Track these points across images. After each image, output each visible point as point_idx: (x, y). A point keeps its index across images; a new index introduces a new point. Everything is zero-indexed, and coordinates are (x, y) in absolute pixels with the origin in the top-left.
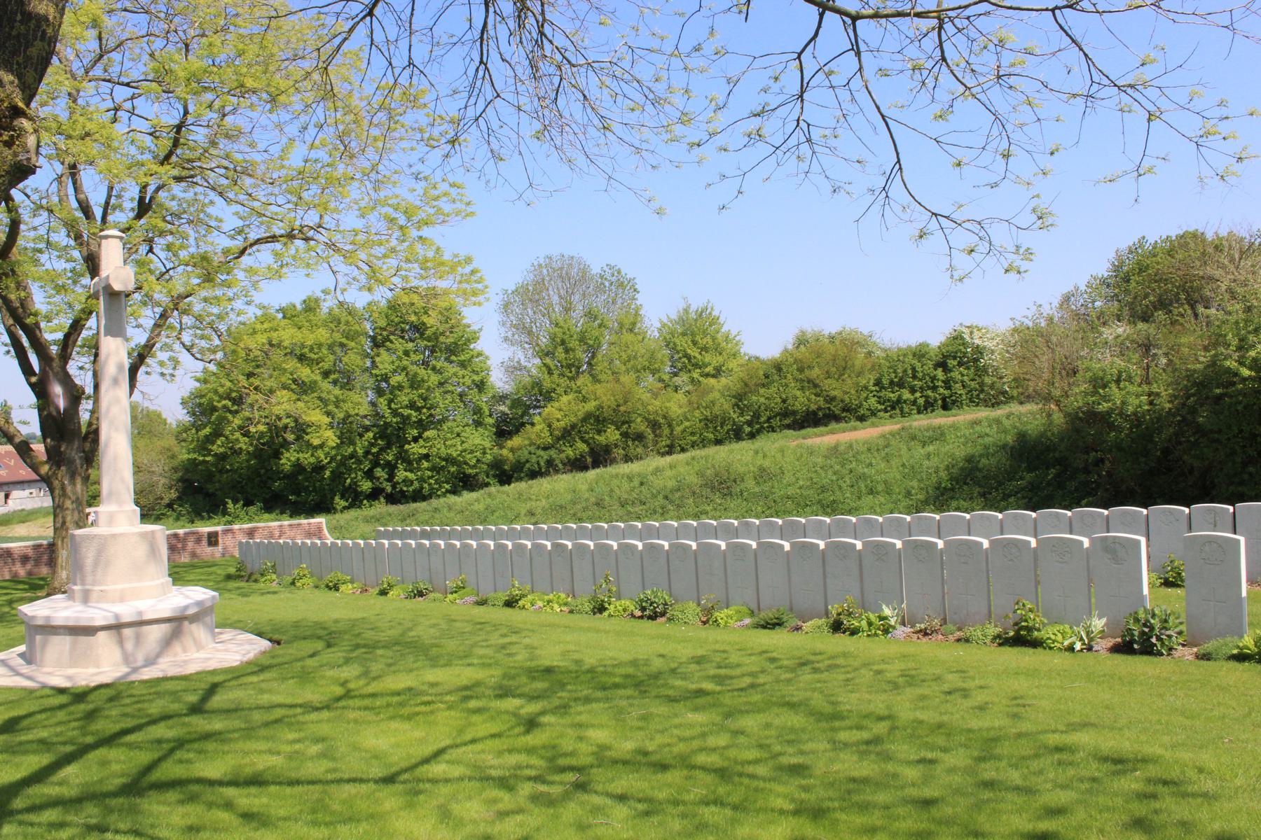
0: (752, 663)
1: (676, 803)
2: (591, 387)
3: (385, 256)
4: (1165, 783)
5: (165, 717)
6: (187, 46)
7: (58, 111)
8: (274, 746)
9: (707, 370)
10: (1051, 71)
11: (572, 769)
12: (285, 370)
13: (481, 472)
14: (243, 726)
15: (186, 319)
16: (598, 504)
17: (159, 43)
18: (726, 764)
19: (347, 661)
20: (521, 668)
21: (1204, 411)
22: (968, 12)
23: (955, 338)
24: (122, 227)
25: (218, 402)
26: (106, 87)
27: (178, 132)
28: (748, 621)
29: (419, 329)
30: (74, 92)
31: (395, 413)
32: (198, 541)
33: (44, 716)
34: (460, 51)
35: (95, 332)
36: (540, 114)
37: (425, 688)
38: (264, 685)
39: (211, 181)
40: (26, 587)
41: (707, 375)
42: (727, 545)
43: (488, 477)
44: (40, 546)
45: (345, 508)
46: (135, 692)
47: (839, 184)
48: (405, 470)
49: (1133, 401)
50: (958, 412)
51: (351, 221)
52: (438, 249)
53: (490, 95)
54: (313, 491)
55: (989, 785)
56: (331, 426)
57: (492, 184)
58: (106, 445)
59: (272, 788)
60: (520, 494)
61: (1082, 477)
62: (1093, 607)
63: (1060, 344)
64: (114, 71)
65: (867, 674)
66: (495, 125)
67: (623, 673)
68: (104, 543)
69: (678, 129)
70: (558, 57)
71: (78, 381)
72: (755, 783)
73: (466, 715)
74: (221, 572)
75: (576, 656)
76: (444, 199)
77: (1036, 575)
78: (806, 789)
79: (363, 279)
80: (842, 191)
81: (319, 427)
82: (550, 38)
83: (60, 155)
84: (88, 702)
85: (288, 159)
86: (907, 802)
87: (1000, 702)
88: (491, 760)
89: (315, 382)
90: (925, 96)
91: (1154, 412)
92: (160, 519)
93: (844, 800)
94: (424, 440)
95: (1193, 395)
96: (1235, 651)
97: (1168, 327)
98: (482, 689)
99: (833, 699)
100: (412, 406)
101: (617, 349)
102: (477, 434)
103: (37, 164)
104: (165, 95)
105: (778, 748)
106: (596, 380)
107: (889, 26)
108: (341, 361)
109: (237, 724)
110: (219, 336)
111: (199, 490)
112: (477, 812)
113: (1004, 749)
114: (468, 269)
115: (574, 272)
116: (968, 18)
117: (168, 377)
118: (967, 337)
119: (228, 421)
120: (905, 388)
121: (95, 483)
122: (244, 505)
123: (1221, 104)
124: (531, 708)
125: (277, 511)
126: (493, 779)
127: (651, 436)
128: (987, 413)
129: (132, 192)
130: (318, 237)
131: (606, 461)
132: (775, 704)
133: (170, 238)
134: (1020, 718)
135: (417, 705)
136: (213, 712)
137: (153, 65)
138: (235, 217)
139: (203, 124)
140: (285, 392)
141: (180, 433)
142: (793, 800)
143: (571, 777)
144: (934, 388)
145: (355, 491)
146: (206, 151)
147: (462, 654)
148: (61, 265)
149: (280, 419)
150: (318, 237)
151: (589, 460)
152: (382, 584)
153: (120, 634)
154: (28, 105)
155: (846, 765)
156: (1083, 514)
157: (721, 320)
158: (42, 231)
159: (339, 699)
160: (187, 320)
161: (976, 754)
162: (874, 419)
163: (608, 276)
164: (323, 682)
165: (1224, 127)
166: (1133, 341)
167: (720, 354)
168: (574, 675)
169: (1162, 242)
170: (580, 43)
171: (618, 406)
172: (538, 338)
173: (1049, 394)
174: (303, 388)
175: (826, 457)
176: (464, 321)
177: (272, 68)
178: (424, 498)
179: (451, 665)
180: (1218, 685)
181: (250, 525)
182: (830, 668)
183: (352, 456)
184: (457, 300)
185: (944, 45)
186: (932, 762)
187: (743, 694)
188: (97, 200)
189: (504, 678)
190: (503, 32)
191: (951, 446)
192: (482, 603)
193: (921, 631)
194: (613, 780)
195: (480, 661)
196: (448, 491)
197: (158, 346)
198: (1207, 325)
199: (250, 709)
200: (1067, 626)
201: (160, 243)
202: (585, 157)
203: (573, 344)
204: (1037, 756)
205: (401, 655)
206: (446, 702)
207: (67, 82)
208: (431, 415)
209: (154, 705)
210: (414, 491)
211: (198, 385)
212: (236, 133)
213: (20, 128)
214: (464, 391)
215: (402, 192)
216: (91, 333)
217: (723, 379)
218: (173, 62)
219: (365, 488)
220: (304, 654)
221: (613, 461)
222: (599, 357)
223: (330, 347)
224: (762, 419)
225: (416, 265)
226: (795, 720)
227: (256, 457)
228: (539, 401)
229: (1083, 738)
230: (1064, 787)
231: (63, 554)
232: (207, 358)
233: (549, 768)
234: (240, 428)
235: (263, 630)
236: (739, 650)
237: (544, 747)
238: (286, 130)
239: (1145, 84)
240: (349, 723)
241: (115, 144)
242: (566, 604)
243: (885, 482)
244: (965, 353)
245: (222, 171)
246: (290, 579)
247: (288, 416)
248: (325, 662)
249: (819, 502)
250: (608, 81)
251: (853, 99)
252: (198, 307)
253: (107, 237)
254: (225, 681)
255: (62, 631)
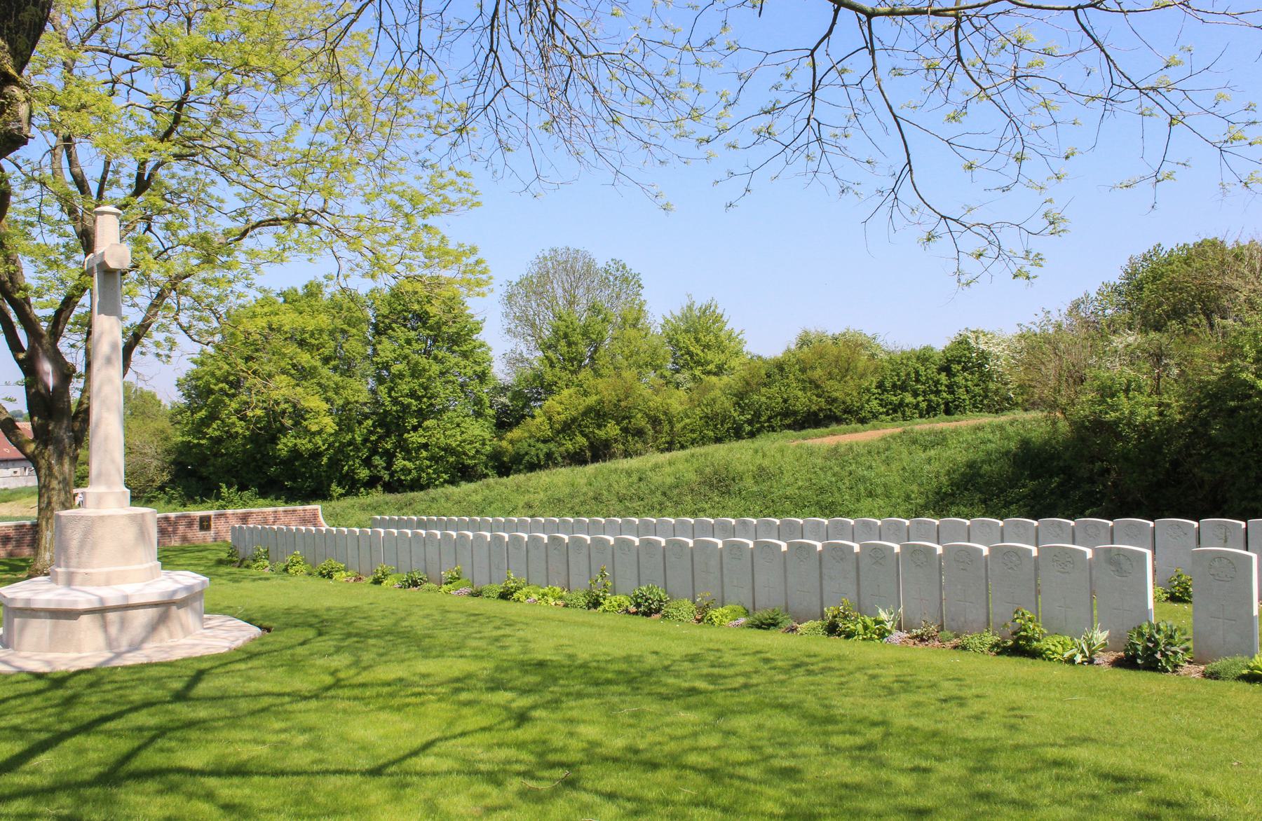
0: (746, 664)
1: (665, 803)
2: (592, 382)
3: (389, 243)
4: (1169, 804)
5: (147, 704)
6: (189, 20)
7: (52, 80)
8: (259, 735)
9: (709, 368)
10: (1071, 74)
11: (562, 765)
12: (285, 355)
13: (479, 463)
14: (228, 714)
15: (183, 300)
16: (595, 499)
17: (159, 16)
18: (716, 765)
19: (338, 650)
20: (514, 661)
21: (1216, 424)
22: (987, 10)
23: (960, 343)
24: (119, 203)
25: (215, 385)
26: (103, 58)
27: (179, 108)
28: (742, 620)
29: (422, 317)
30: (69, 61)
31: (395, 401)
32: (190, 525)
33: (19, 702)
34: (470, 38)
35: (88, 309)
36: (549, 104)
37: (416, 679)
38: (251, 673)
39: (212, 161)
40: (6, 568)
41: (709, 373)
42: (724, 543)
43: (486, 468)
44: (23, 526)
45: (342, 495)
46: (117, 678)
47: (848, 184)
48: (404, 459)
49: (1143, 412)
50: (961, 417)
51: (355, 207)
52: (443, 238)
53: (499, 84)
54: (309, 477)
55: (985, 797)
56: (330, 412)
57: (499, 174)
58: (97, 426)
59: (256, 779)
60: (518, 487)
61: (1087, 487)
62: (1095, 619)
63: (1068, 352)
64: (113, 41)
65: (861, 679)
66: (503, 114)
67: (616, 669)
68: (91, 525)
69: (688, 125)
70: (569, 47)
71: (68, 359)
72: (746, 785)
73: (456, 707)
74: (212, 557)
75: (570, 651)
76: (451, 188)
77: (1037, 585)
78: (797, 793)
79: (366, 265)
80: (850, 191)
81: (318, 413)
82: (562, 27)
83: (54, 126)
84: (67, 688)
85: (293, 141)
86: (900, 811)
87: (997, 712)
88: (480, 753)
89: (315, 368)
90: (938, 97)
91: (1164, 423)
92: (151, 502)
93: (836, 807)
94: (424, 430)
95: (1206, 407)
96: (1245, 672)
97: (1182, 337)
98: (474, 681)
99: (827, 702)
100: (412, 394)
101: (620, 344)
102: (477, 425)
103: (29, 135)
104: (166, 70)
105: (769, 750)
106: (597, 374)
107: (905, 24)
108: (341, 348)
109: (223, 712)
110: (218, 318)
111: (192, 474)
112: (464, 807)
113: (1000, 761)
114: (472, 259)
115: (579, 266)
116: (987, 17)
117: (164, 358)
118: (972, 342)
119: (225, 404)
120: (907, 391)
121: (84, 464)
122: (238, 490)
123: (1249, 108)
124: (523, 702)
125: (273, 497)
126: (482, 773)
127: (651, 433)
128: (990, 419)
129: (129, 168)
130: (321, 221)
131: (605, 456)
132: (768, 705)
133: (169, 217)
134: (1017, 729)
135: (408, 696)
136: (198, 699)
137: (153, 37)
138: (237, 199)
139: (205, 101)
140: (284, 377)
141: (174, 415)
142: (783, 804)
143: (560, 773)
144: (937, 393)
145: (353, 478)
146: (207, 129)
147: (455, 645)
148: (53, 240)
149: (278, 404)
150: (321, 221)
151: (588, 454)
152: (377, 573)
153: (104, 618)
154: (20, 72)
155: (839, 770)
156: (1086, 524)
157: (725, 318)
158: (34, 204)
159: (328, 688)
160: (185, 301)
161: (971, 764)
162: (875, 422)
163: (613, 270)
164: (313, 671)
165: (1250, 134)
166: (1144, 351)
167: (723, 352)
168: (566, 670)
169: (1178, 250)
170: (591, 33)
171: (619, 401)
172: (541, 330)
173: (1055, 402)
174: (303, 374)
175: (826, 458)
176: (467, 312)
177: (277, 47)
178: (422, 488)
179: (443, 656)
180: (1226, 706)
181: (244, 510)
182: (824, 670)
183: (350, 443)
184: (461, 290)
185: (960, 44)
186: (926, 770)
187: (736, 694)
188: (92, 174)
189: (496, 671)
190: (513, 19)
191: (953, 451)
192: (477, 594)
193: (917, 636)
194: (603, 778)
195: (474, 653)
196: (446, 481)
197: (154, 325)
198: (1223, 336)
199: (236, 697)
200: (1068, 638)
201: (159, 221)
202: (593, 150)
203: (576, 337)
204: (1034, 769)
205: (393, 645)
206: (437, 694)
207: (61, 51)
208: (431, 405)
209: (137, 691)
210: (412, 480)
211: (194, 367)
212: (240, 112)
213: (10, 96)
214: (465, 381)
215: (408, 179)
216: (84, 310)
217: (725, 377)
218: (174, 36)
219: (362, 475)
220: (294, 641)
221: (612, 456)
222: (602, 351)
223: (332, 333)
224: (763, 419)
225: (420, 254)
226: (788, 722)
227: (252, 442)
228: (540, 394)
229: (1082, 753)
230: (1062, 803)
231: (47, 536)
232: (204, 340)
233: (539, 764)
234: (237, 411)
235: (254, 616)
236: (733, 649)
237: (534, 742)
238: (291, 111)
239: (1168, 88)
240: (337, 713)
241: (113, 118)
242: (561, 598)
243: (885, 485)
244: (970, 358)
245: (225, 151)
246: (283, 566)
247: (287, 401)
248: (315, 650)
249: (818, 503)
250: (618, 73)
251: (865, 98)
252: (196, 288)
253: (102, 213)
254: (212, 668)
255: (42, 614)
